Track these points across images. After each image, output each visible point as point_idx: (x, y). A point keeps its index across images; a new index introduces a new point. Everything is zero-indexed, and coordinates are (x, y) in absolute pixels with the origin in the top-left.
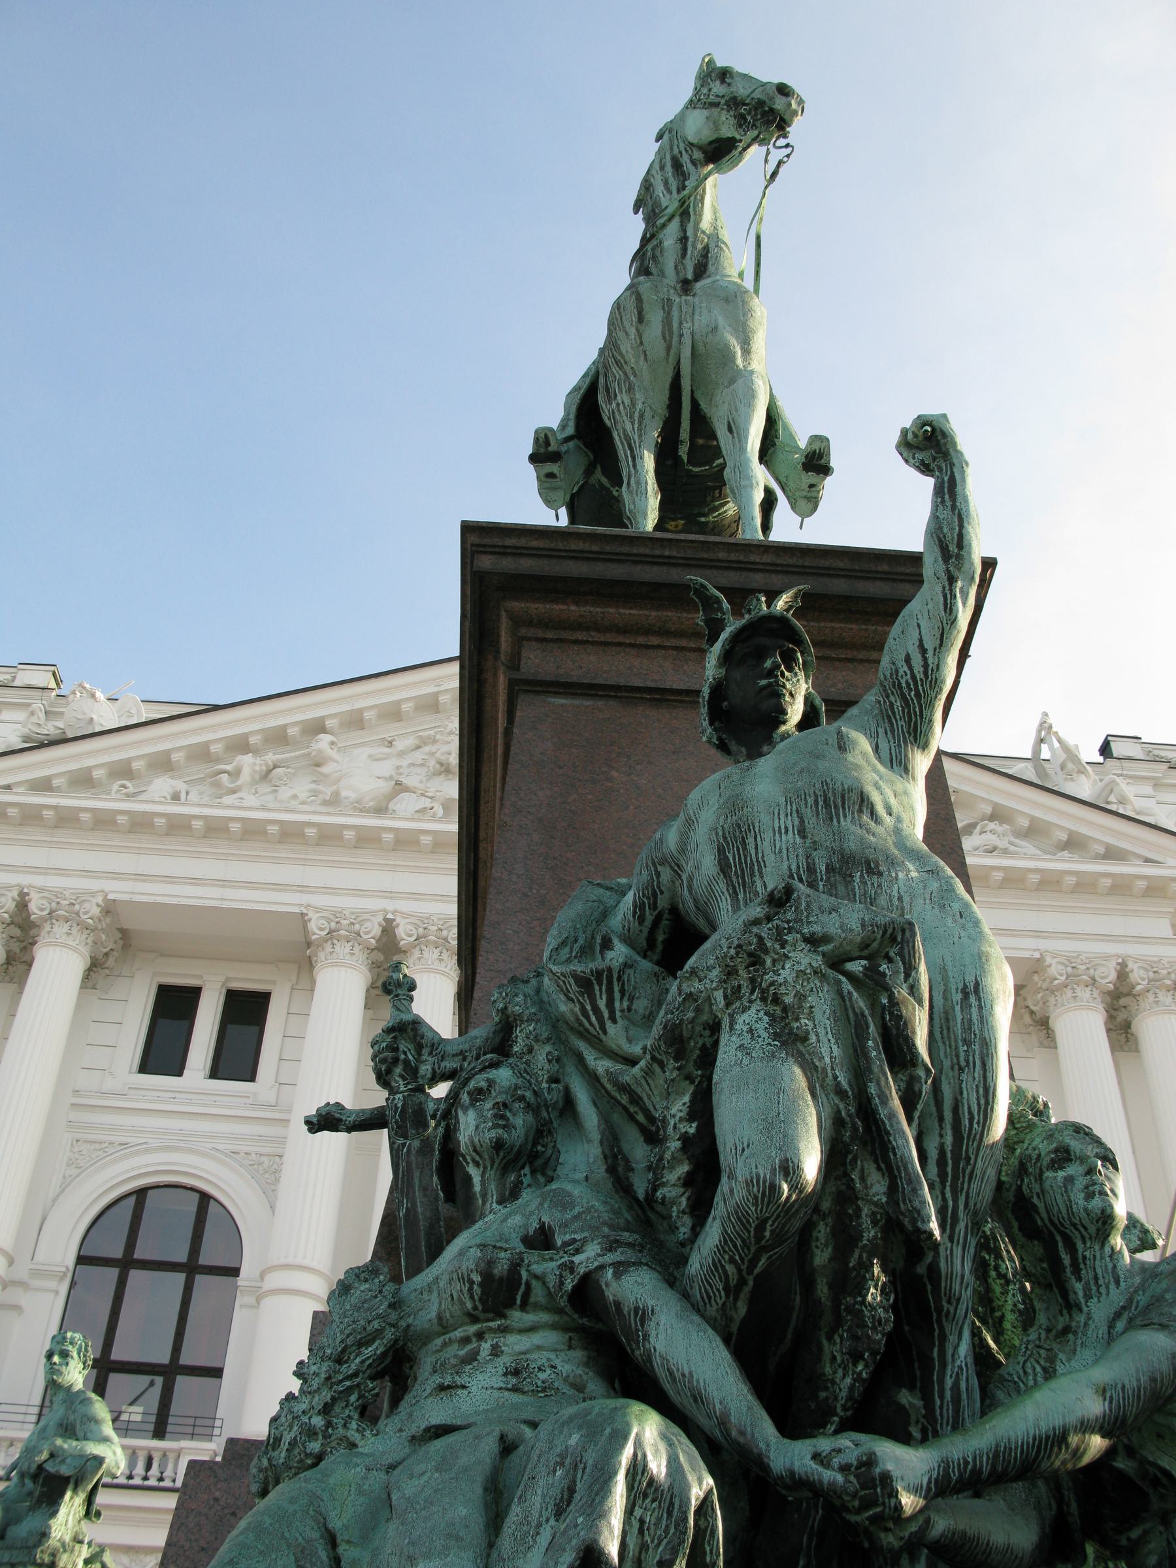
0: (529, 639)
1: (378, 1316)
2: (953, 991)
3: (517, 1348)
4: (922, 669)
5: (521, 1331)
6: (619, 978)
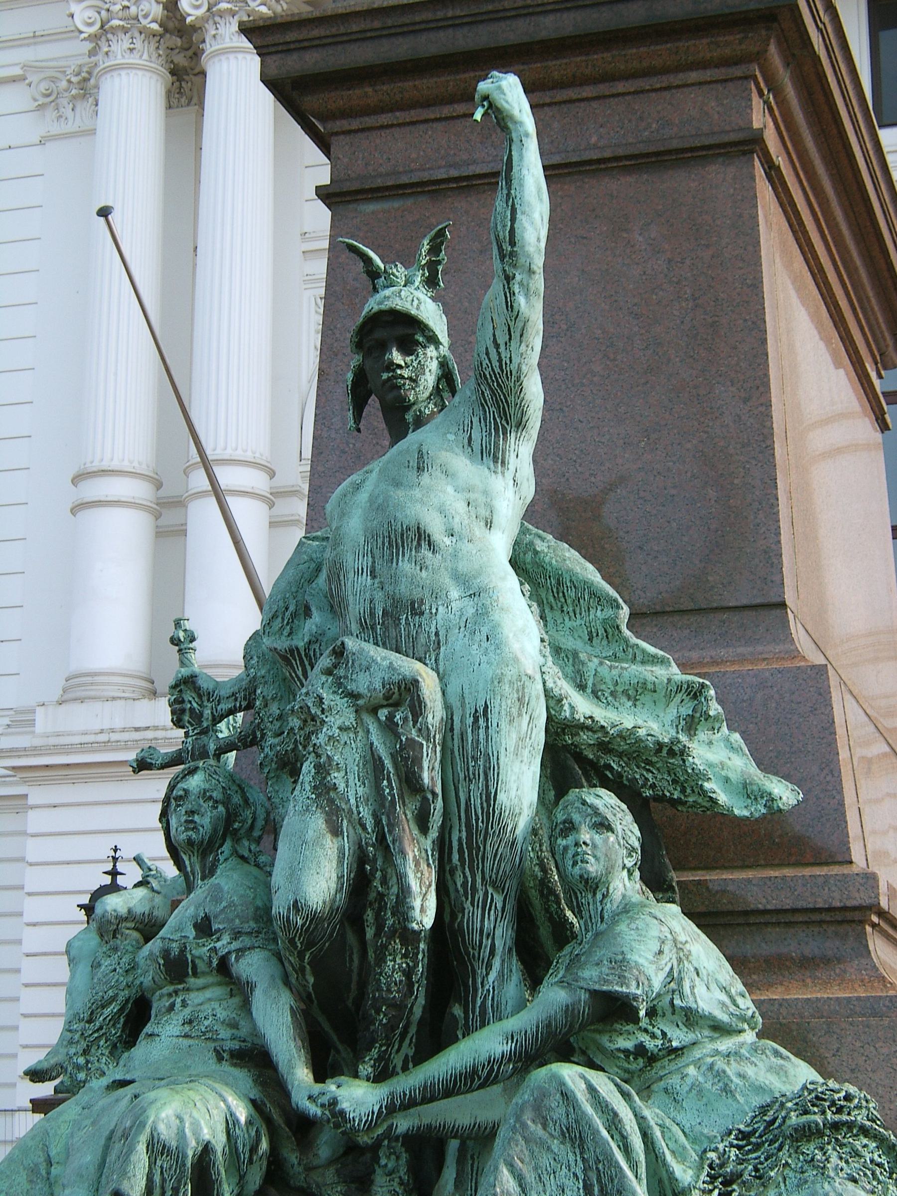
0: (337, 134)
1: (112, 987)
2: (468, 716)
3: (196, 1001)
4: (498, 364)
5: (198, 989)
6: (306, 655)
